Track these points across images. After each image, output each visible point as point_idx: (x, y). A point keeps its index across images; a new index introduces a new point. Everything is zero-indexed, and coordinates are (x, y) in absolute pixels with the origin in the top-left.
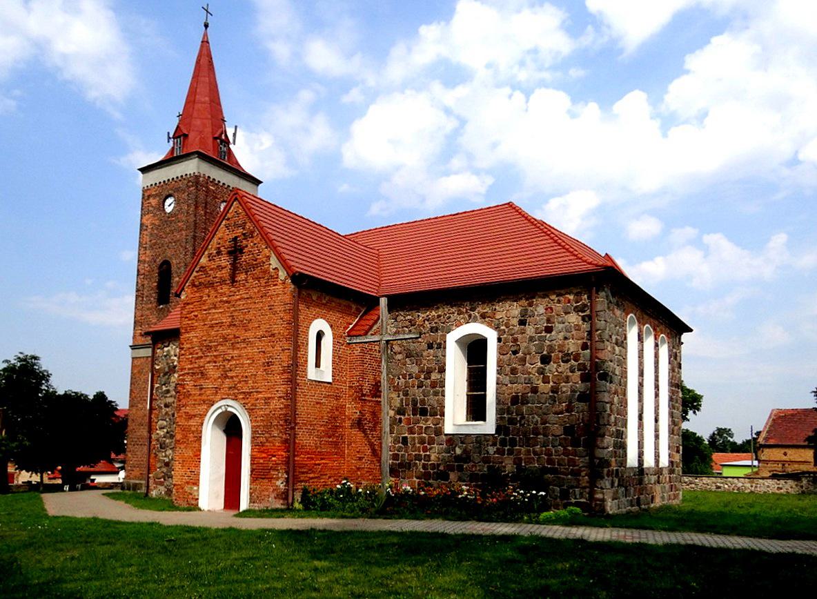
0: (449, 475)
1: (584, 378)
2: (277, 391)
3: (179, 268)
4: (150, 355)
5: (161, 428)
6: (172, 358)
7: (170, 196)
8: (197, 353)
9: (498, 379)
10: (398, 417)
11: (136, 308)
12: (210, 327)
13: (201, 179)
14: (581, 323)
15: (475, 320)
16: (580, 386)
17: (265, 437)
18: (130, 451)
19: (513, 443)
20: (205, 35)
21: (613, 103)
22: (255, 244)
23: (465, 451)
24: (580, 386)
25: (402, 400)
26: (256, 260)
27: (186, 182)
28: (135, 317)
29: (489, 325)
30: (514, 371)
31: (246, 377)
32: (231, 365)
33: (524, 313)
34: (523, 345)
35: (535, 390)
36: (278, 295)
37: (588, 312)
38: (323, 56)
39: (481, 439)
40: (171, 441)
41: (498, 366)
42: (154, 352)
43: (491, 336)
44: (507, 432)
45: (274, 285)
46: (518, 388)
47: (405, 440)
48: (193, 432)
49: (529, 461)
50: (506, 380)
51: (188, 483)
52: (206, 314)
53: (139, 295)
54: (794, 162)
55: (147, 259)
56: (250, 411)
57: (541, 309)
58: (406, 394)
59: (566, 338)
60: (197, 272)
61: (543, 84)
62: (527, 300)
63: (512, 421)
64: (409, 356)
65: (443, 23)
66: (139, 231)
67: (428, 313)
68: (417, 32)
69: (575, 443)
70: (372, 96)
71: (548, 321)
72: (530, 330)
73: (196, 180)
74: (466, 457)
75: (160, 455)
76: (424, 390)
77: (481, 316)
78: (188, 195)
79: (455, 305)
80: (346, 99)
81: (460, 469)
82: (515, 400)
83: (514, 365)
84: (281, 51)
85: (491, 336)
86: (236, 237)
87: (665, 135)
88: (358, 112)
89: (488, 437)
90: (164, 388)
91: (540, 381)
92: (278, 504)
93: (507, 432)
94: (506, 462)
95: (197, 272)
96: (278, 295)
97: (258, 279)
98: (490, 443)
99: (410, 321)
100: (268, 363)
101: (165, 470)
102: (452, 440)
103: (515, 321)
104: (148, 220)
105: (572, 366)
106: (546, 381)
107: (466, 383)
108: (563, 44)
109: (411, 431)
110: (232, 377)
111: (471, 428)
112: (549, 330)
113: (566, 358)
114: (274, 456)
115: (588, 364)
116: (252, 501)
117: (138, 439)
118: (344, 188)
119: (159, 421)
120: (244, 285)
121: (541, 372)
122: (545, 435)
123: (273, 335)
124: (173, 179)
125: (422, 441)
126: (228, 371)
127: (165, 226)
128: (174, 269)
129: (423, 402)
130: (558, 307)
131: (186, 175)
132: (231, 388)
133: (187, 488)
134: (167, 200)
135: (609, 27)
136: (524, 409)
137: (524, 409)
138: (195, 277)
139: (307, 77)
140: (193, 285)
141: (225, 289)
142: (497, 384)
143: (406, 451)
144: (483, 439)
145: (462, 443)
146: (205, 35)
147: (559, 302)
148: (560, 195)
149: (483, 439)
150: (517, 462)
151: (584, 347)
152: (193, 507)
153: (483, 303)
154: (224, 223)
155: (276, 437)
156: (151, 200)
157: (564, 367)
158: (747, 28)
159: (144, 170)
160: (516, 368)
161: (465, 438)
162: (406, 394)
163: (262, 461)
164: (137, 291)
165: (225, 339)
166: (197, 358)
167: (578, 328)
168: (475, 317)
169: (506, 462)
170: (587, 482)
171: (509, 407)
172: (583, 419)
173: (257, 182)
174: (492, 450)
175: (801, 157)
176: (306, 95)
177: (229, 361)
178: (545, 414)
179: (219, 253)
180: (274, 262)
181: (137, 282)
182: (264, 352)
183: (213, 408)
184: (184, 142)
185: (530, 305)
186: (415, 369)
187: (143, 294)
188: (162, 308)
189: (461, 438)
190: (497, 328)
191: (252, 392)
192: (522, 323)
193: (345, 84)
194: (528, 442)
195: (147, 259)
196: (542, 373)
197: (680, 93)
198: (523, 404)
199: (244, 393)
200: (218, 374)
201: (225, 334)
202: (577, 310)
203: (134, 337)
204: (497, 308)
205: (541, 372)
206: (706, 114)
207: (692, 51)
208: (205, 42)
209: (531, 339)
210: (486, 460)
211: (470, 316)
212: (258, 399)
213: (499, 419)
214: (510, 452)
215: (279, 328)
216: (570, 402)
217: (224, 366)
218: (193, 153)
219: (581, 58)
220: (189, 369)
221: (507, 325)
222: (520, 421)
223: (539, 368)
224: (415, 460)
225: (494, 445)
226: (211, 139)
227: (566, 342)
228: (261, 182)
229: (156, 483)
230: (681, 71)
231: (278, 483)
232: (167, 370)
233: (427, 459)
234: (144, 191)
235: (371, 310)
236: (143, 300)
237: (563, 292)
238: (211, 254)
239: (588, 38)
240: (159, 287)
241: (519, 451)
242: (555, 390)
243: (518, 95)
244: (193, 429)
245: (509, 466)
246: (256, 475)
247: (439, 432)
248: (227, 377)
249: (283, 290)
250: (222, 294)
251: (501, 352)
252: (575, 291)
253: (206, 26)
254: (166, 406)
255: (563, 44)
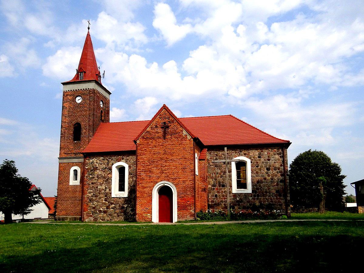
0: (235, 207)
1: (282, 175)
2: (189, 178)
3: (86, 127)
4: (83, 162)
5: (90, 193)
6: (95, 164)
7: (79, 96)
8: (147, 164)
9: (251, 175)
10: (213, 187)
11: (61, 141)
12: (153, 154)
13: (96, 91)
14: (280, 158)
15: (242, 155)
16: (281, 178)
17: (184, 195)
18: (59, 203)
19: (258, 196)
20: (88, 32)
21: (163, 64)
22: (175, 126)
23: (239, 200)
24: (281, 178)
25: (214, 182)
26: (176, 131)
27: (88, 91)
28: (60, 145)
29: (247, 157)
30: (257, 173)
31: (173, 173)
32: (165, 168)
33: (260, 154)
34: (260, 164)
35: (265, 179)
36: (187, 144)
37: (282, 155)
38: (34, 24)
39: (246, 195)
40: (95, 198)
41: (251, 171)
42: (84, 160)
43: (248, 161)
44: (256, 192)
45: (185, 141)
46: (259, 178)
47: (216, 196)
48: (146, 193)
49: (265, 201)
50: (255, 175)
51: (144, 213)
52: (151, 149)
53: (63, 135)
54: (227, 95)
55: (67, 121)
56: (176, 185)
57: (266, 153)
58: (216, 180)
59: (275, 163)
60: (145, 133)
61: (135, 53)
62: (260, 150)
63: (257, 189)
64: (216, 166)
65: (93, 21)
66: (62, 108)
67: (223, 152)
68: (82, 22)
69: (280, 195)
70: (60, 46)
71: (268, 157)
72: (262, 160)
73: (94, 91)
74: (241, 201)
75: (90, 204)
76: (223, 178)
77: (244, 154)
78: (90, 97)
79: (234, 150)
80: (46, 45)
81: (239, 205)
82: (258, 182)
83: (257, 171)
84: (13, 18)
85: (248, 161)
86: (165, 122)
87: (182, 79)
88: (52, 52)
89: (249, 194)
90: (91, 176)
91: (267, 176)
92: (192, 218)
93: (256, 192)
94: (256, 202)
95: (145, 133)
96: (187, 144)
97: (177, 138)
98: (250, 196)
99: (216, 155)
100: (184, 168)
101: (93, 210)
102: (235, 195)
103: (257, 157)
104: (67, 105)
105: (277, 171)
106: (269, 176)
107: (236, 176)
108: (144, 39)
109: (218, 192)
110: (166, 173)
111: (240, 191)
112: (269, 160)
113: (275, 169)
114: (189, 201)
115: (283, 171)
116: (354, 202)
117: (64, 198)
118: (43, 84)
119: (88, 190)
120: (170, 140)
121: (267, 173)
122: (270, 193)
123: (185, 158)
124: (81, 89)
125: (223, 196)
126: (164, 171)
127: (77, 108)
128: (82, 126)
129: (223, 182)
130: (272, 153)
131: (89, 89)
132: (166, 177)
133: (144, 215)
134: (77, 98)
135: (162, 36)
136: (262, 185)
137: (262, 185)
138: (144, 135)
139: (27, 32)
140: (143, 138)
141: (160, 140)
142: (252, 177)
143: (217, 199)
144: (247, 195)
145: (239, 196)
146: (88, 32)
147: (272, 151)
148: (141, 98)
149: (247, 195)
150: (260, 202)
151: (281, 166)
152: (151, 221)
153: (245, 150)
154: (158, 116)
155: (189, 194)
156: (68, 97)
157: (274, 172)
158: (211, 45)
159: (64, 84)
160: (258, 172)
161: (240, 195)
162: (216, 180)
163: (182, 203)
164: (61, 134)
165: (162, 159)
166: (147, 165)
167: (279, 160)
168: (242, 154)
169: (256, 202)
170: (285, 208)
171: (256, 184)
172: (282, 188)
173: (110, 93)
174: (250, 198)
175: (229, 93)
176: (25, 40)
177: (164, 167)
178: (269, 186)
179: (156, 127)
180: (185, 133)
181: (61, 131)
182: (182, 164)
183: (157, 185)
184: (84, 75)
185: (262, 151)
186: (219, 171)
187: (65, 136)
188: (76, 143)
189: (239, 195)
190: (250, 158)
191: (177, 178)
192: (259, 157)
193: (46, 39)
194: (264, 196)
195: (67, 121)
196: (267, 174)
197: (188, 63)
198: (261, 183)
199: (173, 179)
200: (158, 172)
201: (162, 157)
202: (278, 154)
203: (60, 154)
204: (250, 152)
205: (267, 173)
206: (122, 56)
207: (192, 50)
208: (88, 35)
209: (263, 162)
210: (248, 202)
211: (240, 154)
212: (179, 181)
213: (253, 188)
214: (257, 199)
215: (188, 156)
216: (278, 183)
217: (162, 169)
218: (93, 80)
219: (151, 45)
220: (143, 169)
221: (254, 158)
222: (260, 189)
223: (266, 172)
224: (221, 202)
225: (251, 196)
226: (95, 75)
227: (275, 164)
228: (111, 94)
229: (87, 216)
230: (188, 56)
231: (191, 211)
232: (92, 169)
233: (226, 202)
234: (64, 92)
235: (202, 150)
236: (65, 138)
237: (273, 148)
238: (152, 127)
239: (155, 39)
240: (74, 133)
241: (261, 199)
242: (272, 179)
243: (125, 56)
244: (146, 192)
245: (257, 204)
246: (179, 208)
247: (230, 192)
248: (163, 173)
249: (189, 143)
250: (159, 142)
251: (252, 166)
252: (277, 148)
253: (89, 28)
254: (92, 183)
255: (144, 39)
